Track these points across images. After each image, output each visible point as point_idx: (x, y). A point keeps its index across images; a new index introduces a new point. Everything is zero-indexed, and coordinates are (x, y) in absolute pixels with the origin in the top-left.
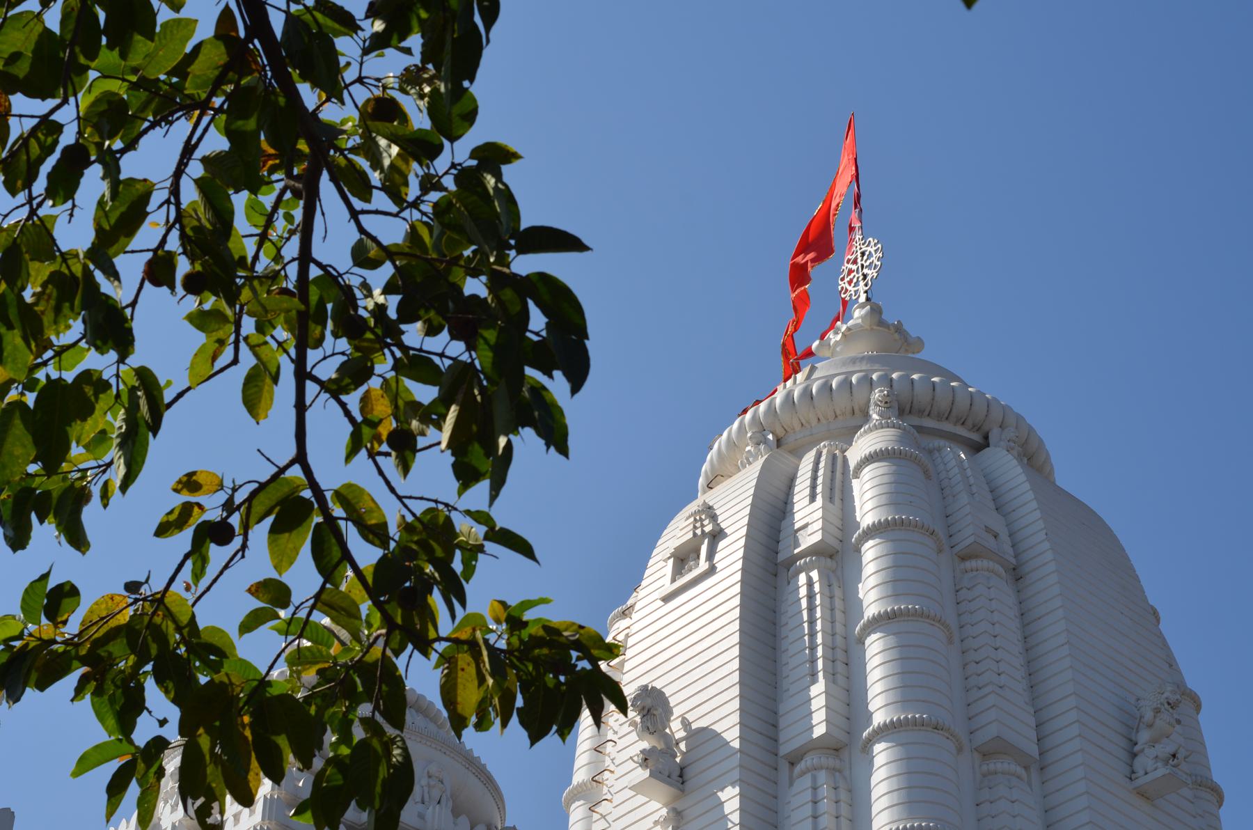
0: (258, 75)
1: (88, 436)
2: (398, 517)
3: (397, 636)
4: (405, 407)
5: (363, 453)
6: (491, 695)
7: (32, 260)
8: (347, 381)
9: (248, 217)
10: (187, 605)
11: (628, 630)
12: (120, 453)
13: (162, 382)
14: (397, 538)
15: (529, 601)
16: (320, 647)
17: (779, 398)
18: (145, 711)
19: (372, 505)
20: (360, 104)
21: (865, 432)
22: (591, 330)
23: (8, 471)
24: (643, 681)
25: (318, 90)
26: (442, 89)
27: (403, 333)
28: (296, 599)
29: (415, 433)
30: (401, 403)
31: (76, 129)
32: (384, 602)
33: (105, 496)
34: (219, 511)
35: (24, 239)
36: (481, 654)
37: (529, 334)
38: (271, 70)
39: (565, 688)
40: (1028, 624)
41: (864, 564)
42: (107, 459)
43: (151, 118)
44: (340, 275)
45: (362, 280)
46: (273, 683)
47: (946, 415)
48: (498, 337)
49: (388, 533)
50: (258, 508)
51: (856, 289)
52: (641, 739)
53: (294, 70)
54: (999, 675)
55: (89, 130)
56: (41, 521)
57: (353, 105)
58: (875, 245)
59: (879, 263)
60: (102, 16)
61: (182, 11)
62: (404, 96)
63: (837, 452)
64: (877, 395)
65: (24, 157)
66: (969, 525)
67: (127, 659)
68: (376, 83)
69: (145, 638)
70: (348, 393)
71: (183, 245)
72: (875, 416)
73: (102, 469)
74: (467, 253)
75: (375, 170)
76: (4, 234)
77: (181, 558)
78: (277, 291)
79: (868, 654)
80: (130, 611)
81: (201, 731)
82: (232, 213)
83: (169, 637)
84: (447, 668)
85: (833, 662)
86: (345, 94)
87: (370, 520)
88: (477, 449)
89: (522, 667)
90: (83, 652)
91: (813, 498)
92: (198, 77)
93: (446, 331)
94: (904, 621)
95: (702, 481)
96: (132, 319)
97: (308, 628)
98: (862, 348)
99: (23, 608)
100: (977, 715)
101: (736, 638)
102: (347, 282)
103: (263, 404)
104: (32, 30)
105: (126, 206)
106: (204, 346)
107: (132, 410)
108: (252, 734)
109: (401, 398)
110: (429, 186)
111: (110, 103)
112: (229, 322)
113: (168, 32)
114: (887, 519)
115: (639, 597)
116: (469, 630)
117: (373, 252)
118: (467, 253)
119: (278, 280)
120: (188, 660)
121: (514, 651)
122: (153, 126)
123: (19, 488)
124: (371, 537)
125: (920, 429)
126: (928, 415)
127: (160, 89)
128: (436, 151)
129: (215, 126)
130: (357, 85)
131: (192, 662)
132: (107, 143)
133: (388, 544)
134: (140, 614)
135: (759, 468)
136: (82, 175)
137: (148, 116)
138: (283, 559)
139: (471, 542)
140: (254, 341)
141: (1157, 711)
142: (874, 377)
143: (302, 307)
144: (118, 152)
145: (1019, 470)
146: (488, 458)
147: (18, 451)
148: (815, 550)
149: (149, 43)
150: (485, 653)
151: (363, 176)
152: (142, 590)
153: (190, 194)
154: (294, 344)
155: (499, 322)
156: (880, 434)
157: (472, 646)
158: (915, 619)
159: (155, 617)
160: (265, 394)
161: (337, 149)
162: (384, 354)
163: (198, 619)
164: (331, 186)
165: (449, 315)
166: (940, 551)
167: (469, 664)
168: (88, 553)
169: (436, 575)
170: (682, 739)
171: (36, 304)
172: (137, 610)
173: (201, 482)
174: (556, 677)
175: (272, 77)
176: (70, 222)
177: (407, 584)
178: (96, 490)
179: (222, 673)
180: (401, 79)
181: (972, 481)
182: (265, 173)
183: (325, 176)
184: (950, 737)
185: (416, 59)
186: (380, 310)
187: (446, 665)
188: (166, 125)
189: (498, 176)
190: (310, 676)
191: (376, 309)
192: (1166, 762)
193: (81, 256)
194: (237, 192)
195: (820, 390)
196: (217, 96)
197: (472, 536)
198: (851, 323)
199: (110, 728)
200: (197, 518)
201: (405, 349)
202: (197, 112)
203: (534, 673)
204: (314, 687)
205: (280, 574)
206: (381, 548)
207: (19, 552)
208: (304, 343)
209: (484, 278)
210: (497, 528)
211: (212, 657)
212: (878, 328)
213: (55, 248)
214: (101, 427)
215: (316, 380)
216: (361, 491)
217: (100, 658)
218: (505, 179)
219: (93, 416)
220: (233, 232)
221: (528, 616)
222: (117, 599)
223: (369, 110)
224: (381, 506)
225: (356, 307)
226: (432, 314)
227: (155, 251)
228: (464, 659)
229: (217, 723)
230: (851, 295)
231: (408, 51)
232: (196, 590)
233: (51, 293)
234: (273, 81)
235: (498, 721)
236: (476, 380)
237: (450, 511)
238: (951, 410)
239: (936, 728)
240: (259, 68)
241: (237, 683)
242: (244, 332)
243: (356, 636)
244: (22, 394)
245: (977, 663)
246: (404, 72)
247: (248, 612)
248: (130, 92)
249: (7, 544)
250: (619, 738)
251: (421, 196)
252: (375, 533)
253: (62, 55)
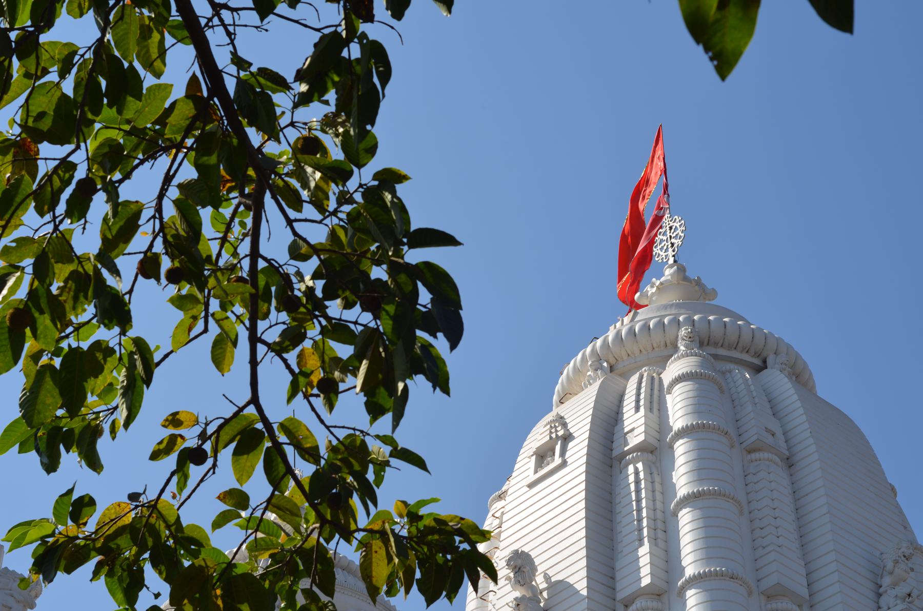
0: (217, 123)
1: (100, 388)
2: (326, 442)
3: (327, 529)
4: (329, 362)
5: (300, 395)
6: (397, 570)
7: (56, 262)
8: (287, 343)
9: (213, 225)
10: (174, 509)
11: (503, 510)
12: (123, 400)
13: (152, 348)
14: (326, 457)
16: (271, 538)
17: (611, 335)
18: (145, 588)
19: (308, 433)
20: (292, 143)
21: (675, 359)
22: (463, 303)
23: (42, 416)
24: (515, 547)
25: (262, 133)
26: (352, 133)
27: (327, 307)
28: (253, 503)
29: (337, 380)
30: (326, 358)
31: (86, 167)
33: (113, 431)
34: (196, 440)
35: (51, 247)
36: (389, 541)
37: (418, 307)
38: (227, 119)
39: (451, 563)
40: (799, 499)
41: (676, 458)
42: (114, 404)
43: (141, 156)
44: (281, 266)
45: (297, 269)
46: (237, 565)
47: (735, 345)
48: (396, 310)
50: (224, 437)
51: (666, 254)
52: (514, 590)
53: (244, 119)
55: (95, 166)
56: (68, 451)
57: (287, 144)
58: (680, 221)
59: (683, 235)
60: (103, 83)
61: (162, 77)
62: (324, 135)
63: (654, 375)
64: (683, 332)
65: (49, 189)
67: (131, 550)
68: (304, 126)
70: (287, 352)
71: (165, 248)
72: (682, 348)
73: (110, 411)
74: (373, 248)
75: (304, 189)
76: (36, 245)
77: (168, 475)
78: (235, 278)
79: (681, 524)
80: (133, 514)
81: (186, 601)
82: (200, 224)
83: (161, 533)
84: (365, 551)
85: (655, 530)
86: (281, 135)
87: (306, 444)
88: (382, 391)
89: (419, 549)
90: (98, 544)
91: (637, 409)
92: (174, 126)
93: (358, 306)
95: (555, 398)
96: (130, 303)
97: (262, 524)
98: (672, 298)
99: (54, 514)
100: (762, 567)
102: (286, 271)
103: (226, 361)
104: (53, 95)
107: (131, 368)
108: (223, 602)
111: (110, 146)
112: (200, 303)
113: (152, 93)
115: (511, 485)
116: (380, 523)
117: (304, 249)
118: (373, 248)
119: (235, 271)
120: (176, 550)
121: (413, 538)
122: (142, 162)
123: (50, 427)
124: (307, 456)
125: (716, 357)
127: (147, 134)
128: (349, 175)
129: (188, 160)
130: (290, 128)
132: (109, 177)
135: (597, 388)
136: (91, 200)
138: (243, 474)
140: (218, 316)
141: (896, 562)
142: (681, 319)
143: (253, 291)
144: (116, 182)
145: (789, 385)
147: (49, 401)
148: (639, 448)
149: (138, 102)
150: (392, 540)
151: (296, 193)
152: (141, 499)
153: (169, 211)
154: (248, 317)
157: (383, 534)
158: (715, 497)
159: (151, 518)
160: (228, 354)
161: (277, 174)
162: (313, 323)
163: (182, 519)
164: (273, 201)
166: (732, 447)
169: (355, 483)
170: (544, 589)
171: (60, 295)
172: (138, 513)
173: (182, 420)
174: (444, 556)
175: (227, 125)
176: (83, 233)
177: (334, 491)
178: (106, 427)
179: (200, 558)
180: (322, 123)
181: (755, 394)
182: (225, 193)
183: (268, 195)
184: (743, 584)
185: (332, 108)
186: (310, 291)
187: (364, 549)
188: (152, 160)
190: (264, 561)
192: (904, 600)
193: (92, 259)
194: (203, 207)
195: (641, 329)
196: (188, 138)
197: (381, 454)
198: (663, 279)
199: (119, 599)
200: (181, 446)
201: (329, 319)
202: (174, 151)
203: (428, 553)
204: (267, 567)
205: (241, 485)
207: (52, 474)
208: (255, 317)
209: (385, 267)
210: (399, 448)
211: (193, 547)
213: (73, 254)
214: (109, 381)
215: (264, 343)
217: (111, 549)
218: (399, 194)
219: (103, 374)
220: (202, 238)
221: (422, 512)
222: (123, 506)
224: (313, 433)
225: (292, 289)
226: (348, 293)
227: (145, 253)
228: (377, 544)
229: (197, 595)
230: (662, 259)
231: (327, 103)
233: (71, 286)
234: (228, 127)
235: (402, 590)
236: (380, 341)
237: (364, 436)
239: (732, 578)
240: (218, 118)
241: (211, 566)
242: (211, 310)
243: (297, 529)
244: (51, 359)
247: (218, 513)
248: (125, 137)
249: (43, 468)
250: (498, 589)
251: (338, 208)
252: (311, 454)
253: (75, 113)
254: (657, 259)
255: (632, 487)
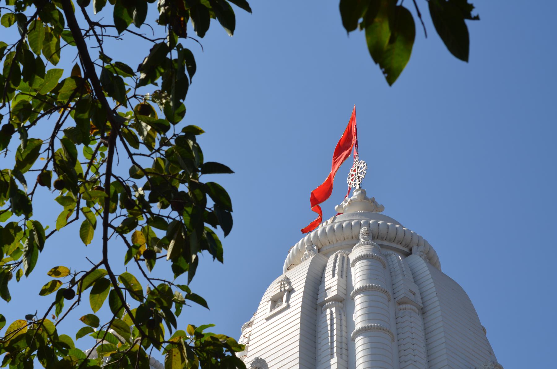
2: (147, 288)
3: (146, 340)
5: (133, 259)
8: (126, 228)
12: (26, 258)
13: (44, 227)
14: (147, 297)
15: (205, 326)
16: (112, 344)
21: (357, 246)
22: (234, 207)
24: (256, 356)
27: (151, 207)
28: (101, 323)
29: (156, 252)
30: (149, 238)
31: (9, 117)
32: (141, 325)
33: (18, 276)
34: (68, 284)
36: (183, 349)
37: (206, 209)
39: (220, 364)
40: (428, 333)
42: (19, 260)
44: (124, 181)
45: (134, 183)
47: (393, 240)
48: (193, 211)
49: (143, 295)
50: (86, 283)
51: (355, 183)
54: (414, 356)
55: (14, 117)
58: (364, 164)
59: (365, 172)
60: (22, 67)
61: (57, 65)
63: (345, 255)
64: (363, 230)
66: (402, 289)
67: (26, 349)
68: (142, 98)
69: (34, 340)
70: (126, 233)
71: (55, 168)
72: (362, 240)
73: (17, 264)
77: (51, 305)
78: (96, 188)
79: (357, 346)
80: (28, 328)
82: (76, 154)
84: (168, 355)
85: (341, 349)
87: (135, 289)
89: (201, 354)
90: (6, 345)
91: (333, 275)
92: (63, 94)
94: (373, 331)
95: (285, 267)
96: (31, 200)
97: (107, 336)
98: (357, 209)
101: (298, 337)
102: (127, 184)
103: (89, 237)
105: (30, 150)
106: (63, 212)
107: (31, 240)
109: (150, 236)
110: (163, 144)
111: (24, 105)
114: (366, 285)
115: (256, 318)
116: (178, 338)
117: (139, 172)
122: (43, 115)
124: (135, 296)
126: (385, 240)
128: (167, 128)
130: (133, 98)
131: (55, 351)
132: (22, 124)
133: (143, 300)
134: (32, 329)
135: (310, 261)
136: (11, 137)
137: (40, 111)
138: (96, 306)
139: (179, 300)
140: (85, 210)
142: (362, 222)
143: (107, 196)
144: (27, 127)
145: (425, 265)
146: (188, 263)
148: (334, 299)
149: (42, 79)
150: (185, 349)
152: (33, 318)
153: (58, 146)
154: (103, 211)
155: (193, 204)
156: (364, 248)
157: (179, 345)
158: (377, 330)
160: (90, 233)
162: (142, 216)
165: (171, 200)
167: (177, 353)
168: (10, 302)
169: (164, 314)
173: (61, 271)
174: (216, 359)
175: (96, 95)
176: (5, 157)
177: (151, 318)
178: (14, 274)
180: (153, 96)
181: (404, 269)
182: (92, 135)
183: (118, 138)
185: (160, 88)
186: (141, 197)
187: (168, 353)
189: (194, 140)
191: (140, 197)
193: (10, 173)
195: (338, 227)
196: (72, 102)
197: (180, 297)
198: (352, 198)
200: (59, 287)
205: (95, 312)
206: (139, 301)
209: (187, 184)
210: (191, 294)
212: (365, 200)
215: (112, 227)
216: (131, 276)
217: (14, 348)
218: (197, 141)
219: (14, 242)
221: (204, 332)
222: (22, 322)
223: (138, 110)
225: (131, 196)
226: (164, 199)
227: (42, 170)
228: (176, 351)
230: (352, 186)
231: (156, 84)
232: (57, 319)
234: (96, 97)
236: (182, 229)
237: (170, 285)
238: (395, 238)
240: (90, 91)
241: (75, 361)
242: (81, 206)
243: (128, 340)
245: (405, 350)
246: (154, 93)
253: (3, 84)
254: (349, 186)
255: (329, 322)
